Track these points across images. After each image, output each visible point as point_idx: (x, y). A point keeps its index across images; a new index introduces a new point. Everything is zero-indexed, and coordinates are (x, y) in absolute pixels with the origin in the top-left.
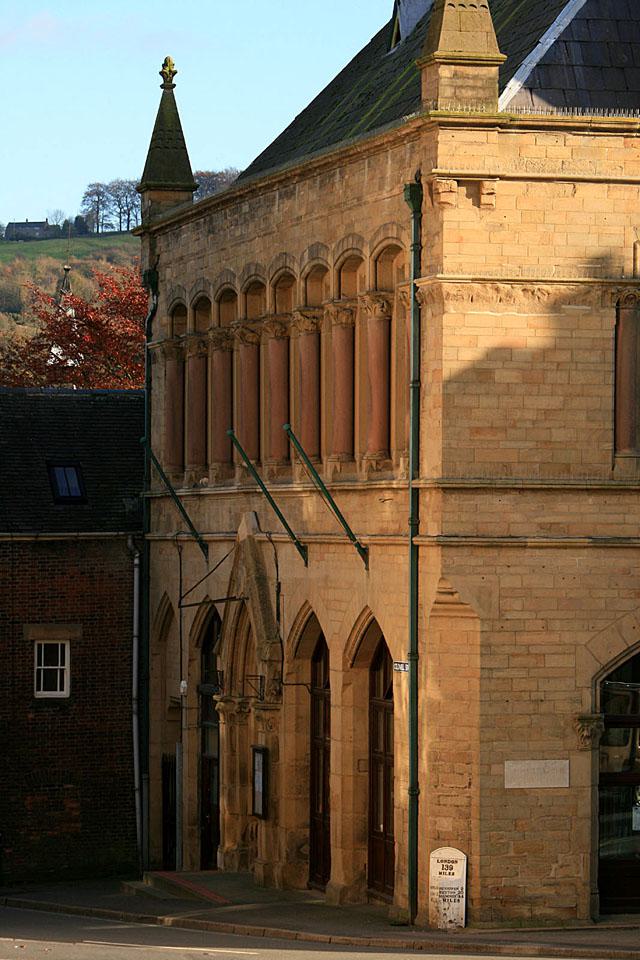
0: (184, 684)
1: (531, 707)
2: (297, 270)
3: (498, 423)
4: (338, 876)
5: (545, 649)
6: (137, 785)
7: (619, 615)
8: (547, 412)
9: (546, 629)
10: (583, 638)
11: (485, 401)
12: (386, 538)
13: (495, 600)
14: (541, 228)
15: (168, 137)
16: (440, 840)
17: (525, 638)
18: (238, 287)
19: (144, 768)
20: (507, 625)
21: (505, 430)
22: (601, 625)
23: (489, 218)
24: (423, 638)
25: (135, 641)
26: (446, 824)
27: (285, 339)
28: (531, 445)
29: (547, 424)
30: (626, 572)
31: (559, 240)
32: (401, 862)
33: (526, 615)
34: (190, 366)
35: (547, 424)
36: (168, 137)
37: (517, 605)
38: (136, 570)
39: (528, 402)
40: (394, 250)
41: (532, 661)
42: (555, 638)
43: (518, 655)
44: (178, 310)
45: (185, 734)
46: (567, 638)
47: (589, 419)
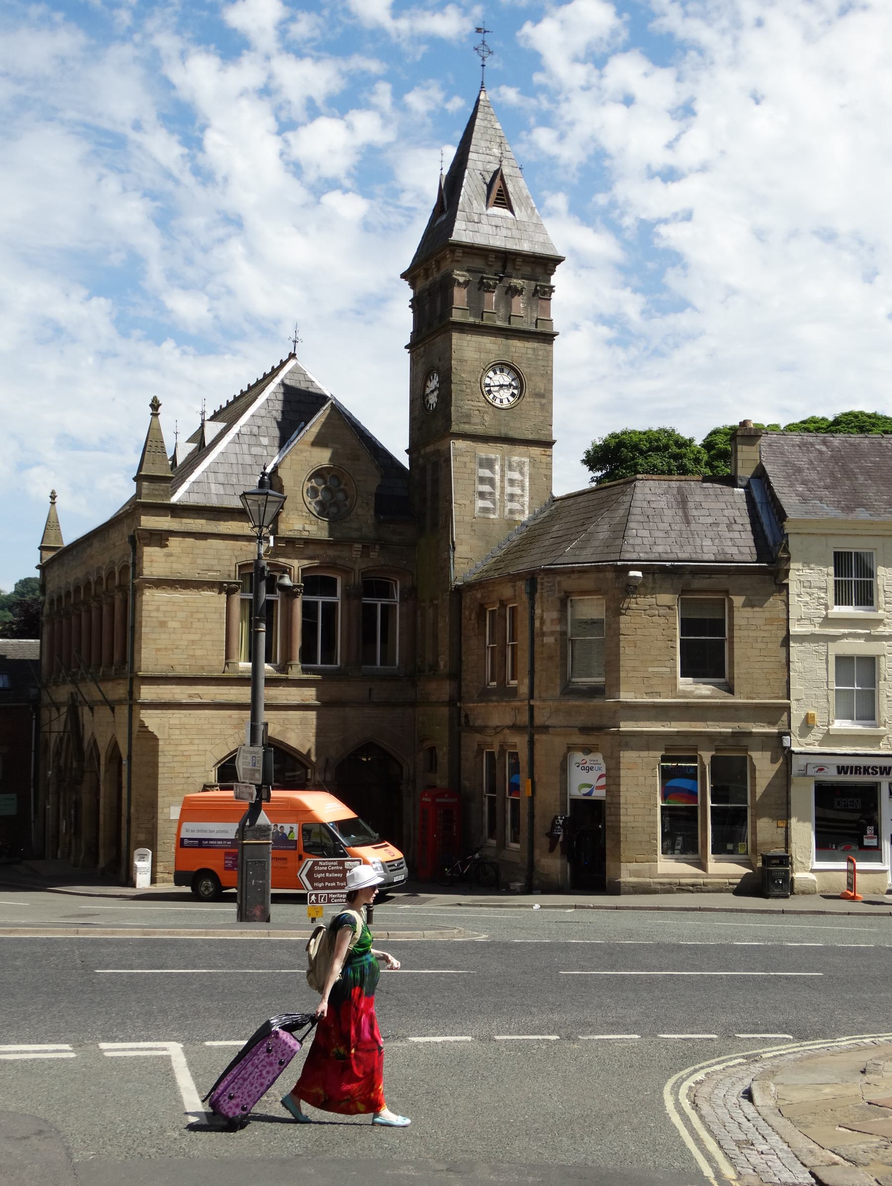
0: (50, 773)
1: (184, 780)
2: (92, 579)
3: (169, 647)
4: (102, 864)
5: (190, 753)
6: (32, 819)
7: (226, 737)
8: (193, 641)
9: (191, 743)
10: (209, 748)
11: (163, 636)
12: (120, 702)
13: (166, 729)
14: (191, 556)
15: (52, 525)
16: (140, 845)
17: (181, 748)
18: (63, 595)
19: (36, 812)
20: (172, 742)
21: (172, 650)
22: (217, 741)
23: (165, 550)
24: (134, 748)
25: (33, 754)
26: (142, 837)
27: (89, 611)
28: (185, 656)
29: (193, 647)
30: (230, 717)
31: (199, 561)
32: (124, 855)
33: (181, 737)
34: (56, 626)
35: (193, 647)
36: (52, 525)
37: (177, 732)
38: (34, 721)
39: (184, 636)
40: (126, 567)
41: (184, 759)
42: (195, 748)
43: (178, 756)
44: (52, 603)
45: (51, 796)
46: (201, 748)
47: (212, 645)
